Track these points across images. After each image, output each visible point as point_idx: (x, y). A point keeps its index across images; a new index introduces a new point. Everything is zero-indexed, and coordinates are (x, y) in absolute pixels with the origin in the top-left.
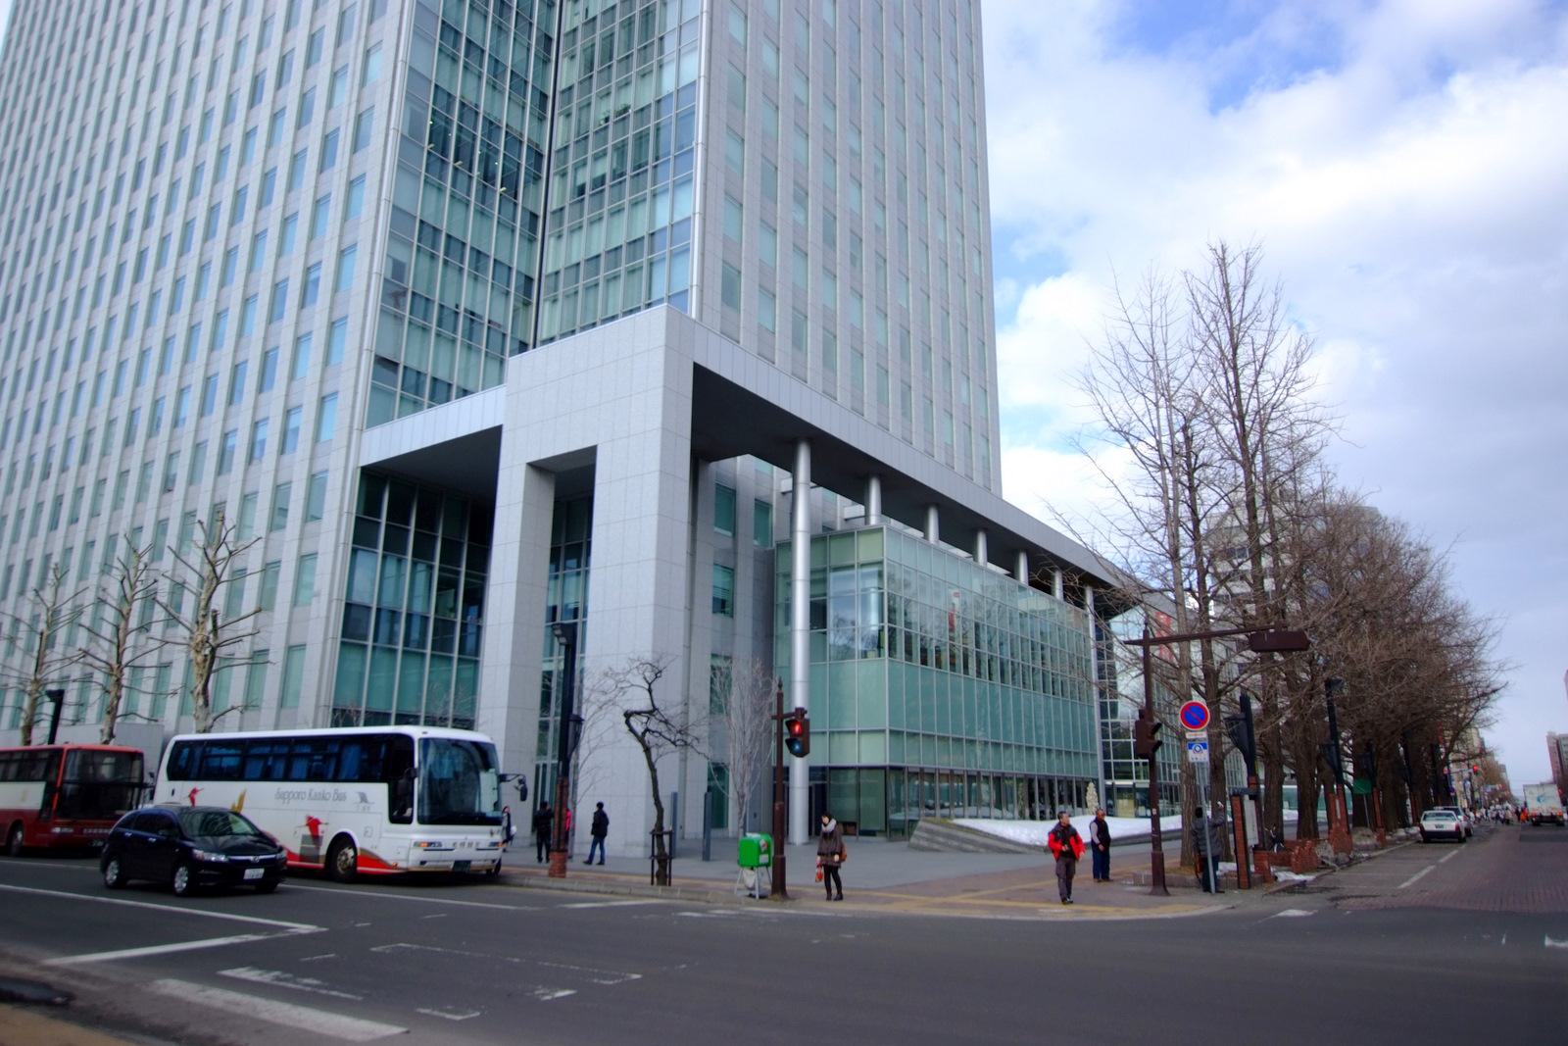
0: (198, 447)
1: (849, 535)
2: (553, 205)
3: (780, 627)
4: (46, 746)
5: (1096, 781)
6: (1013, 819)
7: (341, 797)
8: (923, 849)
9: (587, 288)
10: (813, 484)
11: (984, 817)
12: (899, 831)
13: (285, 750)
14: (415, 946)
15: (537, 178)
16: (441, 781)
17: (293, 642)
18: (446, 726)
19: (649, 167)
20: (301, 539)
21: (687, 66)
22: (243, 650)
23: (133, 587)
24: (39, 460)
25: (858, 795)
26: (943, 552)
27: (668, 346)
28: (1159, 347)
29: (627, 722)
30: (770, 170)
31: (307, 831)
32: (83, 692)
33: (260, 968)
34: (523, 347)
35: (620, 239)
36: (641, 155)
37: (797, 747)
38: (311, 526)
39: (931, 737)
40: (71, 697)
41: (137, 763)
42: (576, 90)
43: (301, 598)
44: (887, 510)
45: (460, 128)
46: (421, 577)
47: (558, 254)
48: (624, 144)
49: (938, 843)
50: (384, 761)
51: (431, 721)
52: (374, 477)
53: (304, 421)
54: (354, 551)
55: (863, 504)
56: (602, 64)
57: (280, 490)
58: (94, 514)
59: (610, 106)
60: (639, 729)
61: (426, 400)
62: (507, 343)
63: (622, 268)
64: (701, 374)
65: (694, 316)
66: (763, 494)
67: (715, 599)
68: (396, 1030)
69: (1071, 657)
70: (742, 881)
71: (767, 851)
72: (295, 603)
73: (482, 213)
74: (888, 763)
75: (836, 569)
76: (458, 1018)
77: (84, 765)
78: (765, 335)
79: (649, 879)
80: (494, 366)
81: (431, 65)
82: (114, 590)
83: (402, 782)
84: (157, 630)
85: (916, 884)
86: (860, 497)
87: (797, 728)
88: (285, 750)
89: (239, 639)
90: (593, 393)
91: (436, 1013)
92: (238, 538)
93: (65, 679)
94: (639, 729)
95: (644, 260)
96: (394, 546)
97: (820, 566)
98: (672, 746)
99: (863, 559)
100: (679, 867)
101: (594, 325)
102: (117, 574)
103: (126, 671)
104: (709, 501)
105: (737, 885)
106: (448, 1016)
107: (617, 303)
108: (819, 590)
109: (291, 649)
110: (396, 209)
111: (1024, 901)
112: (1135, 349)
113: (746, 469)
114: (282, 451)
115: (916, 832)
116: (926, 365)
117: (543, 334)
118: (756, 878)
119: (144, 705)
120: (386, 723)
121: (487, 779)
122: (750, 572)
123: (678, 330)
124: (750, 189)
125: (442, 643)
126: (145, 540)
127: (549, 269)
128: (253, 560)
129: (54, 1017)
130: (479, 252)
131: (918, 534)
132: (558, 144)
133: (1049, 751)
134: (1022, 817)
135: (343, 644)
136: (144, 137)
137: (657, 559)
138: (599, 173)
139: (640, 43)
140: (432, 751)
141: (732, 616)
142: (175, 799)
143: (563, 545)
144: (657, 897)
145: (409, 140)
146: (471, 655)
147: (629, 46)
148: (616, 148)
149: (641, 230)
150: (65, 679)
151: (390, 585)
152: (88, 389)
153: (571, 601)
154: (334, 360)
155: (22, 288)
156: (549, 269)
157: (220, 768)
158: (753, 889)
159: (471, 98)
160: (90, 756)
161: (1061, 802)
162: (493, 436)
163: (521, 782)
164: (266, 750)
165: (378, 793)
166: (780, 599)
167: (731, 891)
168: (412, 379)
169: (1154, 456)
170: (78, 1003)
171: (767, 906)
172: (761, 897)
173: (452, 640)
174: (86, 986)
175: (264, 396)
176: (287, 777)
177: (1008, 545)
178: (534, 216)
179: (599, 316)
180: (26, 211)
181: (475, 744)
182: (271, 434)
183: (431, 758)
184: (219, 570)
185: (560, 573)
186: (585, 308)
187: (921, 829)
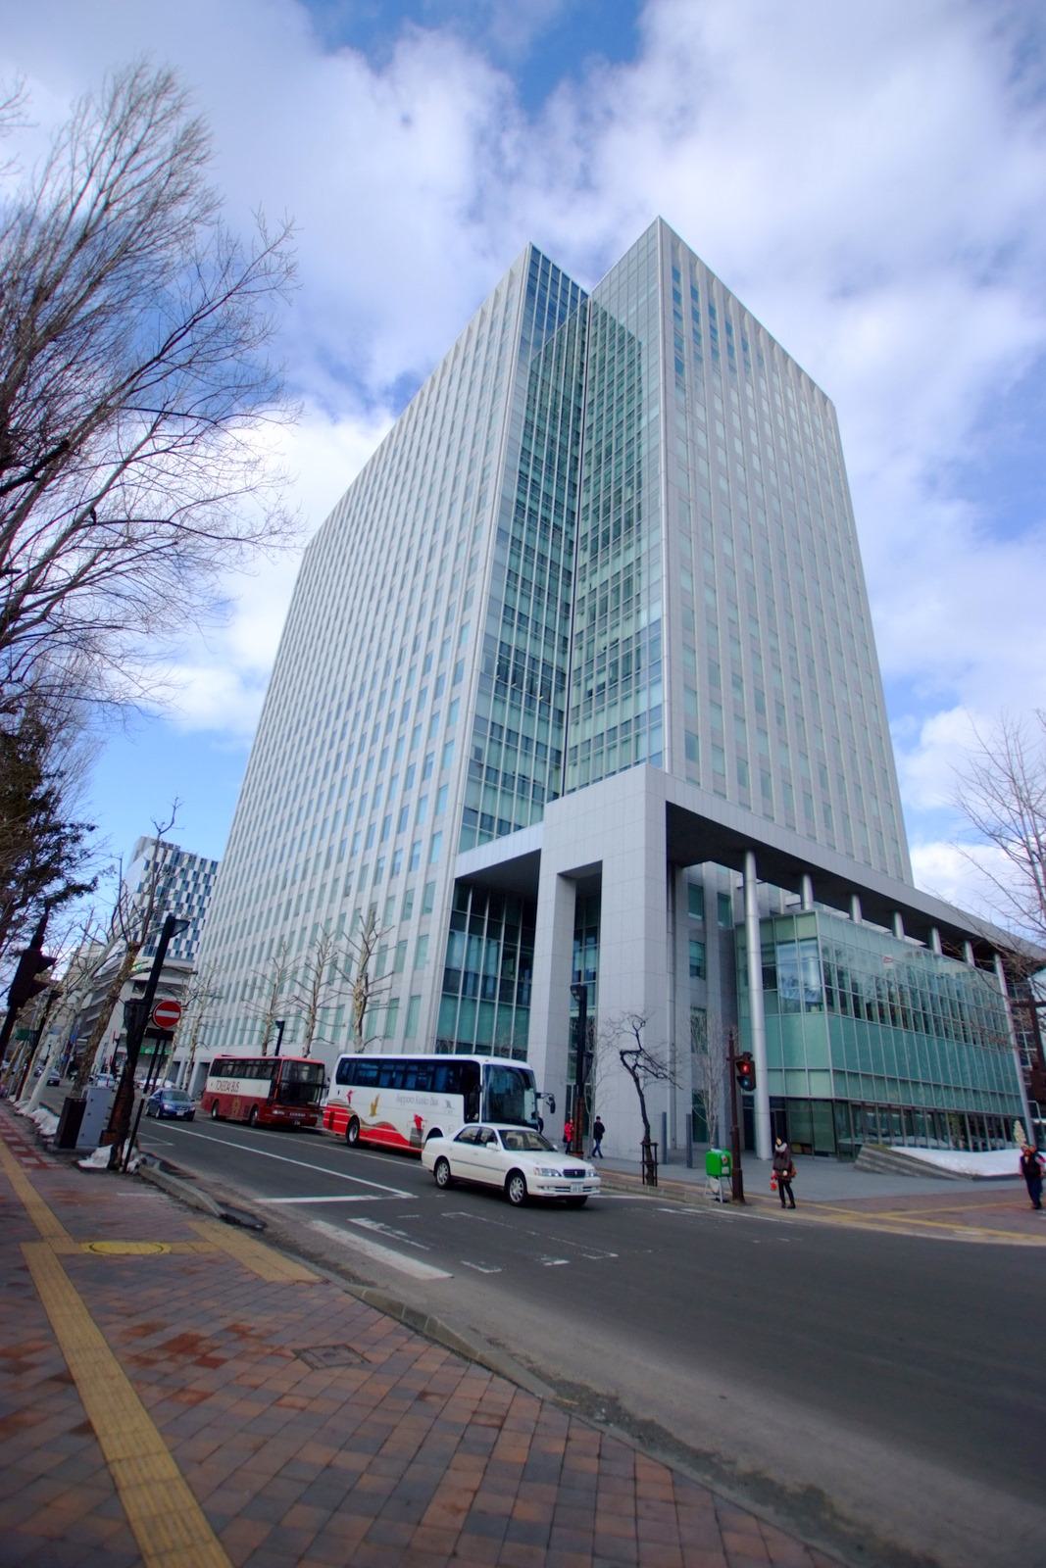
0: (364, 868)
1: (789, 918)
2: (573, 704)
3: (741, 988)
4: (274, 1057)
5: (1022, 1120)
6: (949, 1149)
7: (435, 1103)
8: (867, 1171)
9: (596, 755)
10: (758, 881)
11: (922, 1146)
12: (848, 1154)
13: (402, 1068)
14: (470, 1216)
15: (563, 689)
16: (499, 1095)
17: (414, 994)
18: (507, 1057)
19: (633, 675)
20: (419, 926)
21: (655, 610)
22: (385, 998)
23: (324, 957)
24: (281, 878)
25: (812, 1121)
26: (866, 930)
27: (647, 792)
28: (1016, 771)
29: (622, 1059)
30: (714, 670)
31: (414, 1125)
32: (296, 1022)
33: (372, 1220)
34: (556, 796)
35: (616, 721)
36: (625, 669)
37: (746, 1083)
38: (426, 917)
39: (894, 1080)
40: (289, 1026)
41: (321, 1071)
42: (585, 634)
43: (419, 964)
44: (818, 897)
45: (515, 665)
46: (493, 950)
47: (576, 735)
48: (617, 662)
49: (878, 1166)
50: (460, 1079)
51: (501, 1052)
52: (463, 885)
53: (422, 851)
54: (451, 934)
55: (797, 893)
56: (601, 614)
57: (408, 894)
58: (307, 910)
59: (606, 640)
60: (631, 1064)
61: (495, 834)
62: (541, 795)
63: (618, 741)
64: (671, 809)
65: (667, 771)
66: (723, 889)
67: (691, 966)
68: (446, 1275)
69: (987, 1013)
70: (709, 1186)
71: (727, 1165)
72: (415, 967)
73: (530, 714)
74: (833, 1097)
75: (781, 943)
76: (487, 1271)
77: (292, 1071)
78: (718, 776)
79: (641, 1180)
80: (537, 809)
81: (498, 632)
82: (315, 960)
83: (472, 1094)
84: (337, 984)
85: (854, 1200)
86: (796, 888)
87: (745, 1068)
88: (402, 1068)
89: (380, 992)
90: (599, 825)
91: (473, 1266)
92: (384, 925)
93: (287, 1015)
94: (631, 1064)
95: (632, 734)
96: (475, 929)
97: (769, 941)
98: (655, 1078)
99: (801, 936)
100: (662, 1171)
101: (601, 778)
102: (316, 949)
103: (319, 1011)
104: (680, 891)
105: (706, 1189)
106: (481, 1269)
107: (614, 765)
108: (768, 959)
109: (412, 998)
110: (477, 717)
111: (944, 1222)
112: (995, 772)
113: (710, 872)
114: (410, 870)
115: (860, 1156)
116: (841, 790)
117: (568, 787)
118: (719, 1186)
119: (328, 1035)
120: (469, 1052)
121: (528, 1095)
122: (717, 946)
123: (654, 780)
124: (701, 682)
125: (505, 996)
126: (333, 926)
127: (571, 744)
128: (392, 940)
129: (253, 1237)
130: (527, 738)
131: (844, 915)
132: (575, 666)
133: (1002, 1095)
134: (957, 1148)
135: (443, 995)
136: (343, 690)
137: (646, 939)
138: (601, 682)
139: (625, 598)
140: (492, 1073)
141: (705, 979)
142: (340, 1097)
143: (584, 927)
144: (647, 1194)
145: (485, 675)
146: (524, 1004)
147: (618, 602)
148: (611, 665)
149: (630, 715)
150: (287, 1015)
151: (474, 955)
152: (308, 835)
153: (590, 967)
154: (440, 811)
155: (278, 779)
156: (571, 744)
157: (366, 1078)
158: (717, 1194)
159: (522, 646)
160: (296, 1065)
161: (992, 1136)
162: (535, 856)
163: (551, 1099)
164: (392, 1067)
165: (458, 1101)
166: (741, 966)
167: (701, 1194)
168: (487, 821)
169: (1023, 853)
170: (269, 1230)
171: (726, 1209)
172: (725, 1201)
173: (512, 993)
174: (275, 1219)
175: (400, 836)
176: (403, 1087)
177: (921, 924)
178: (561, 713)
179: (604, 772)
180: (283, 736)
181: (522, 1071)
182: (403, 860)
183: (491, 1077)
184: (370, 946)
185: (583, 948)
186: (595, 767)
187: (864, 1153)
